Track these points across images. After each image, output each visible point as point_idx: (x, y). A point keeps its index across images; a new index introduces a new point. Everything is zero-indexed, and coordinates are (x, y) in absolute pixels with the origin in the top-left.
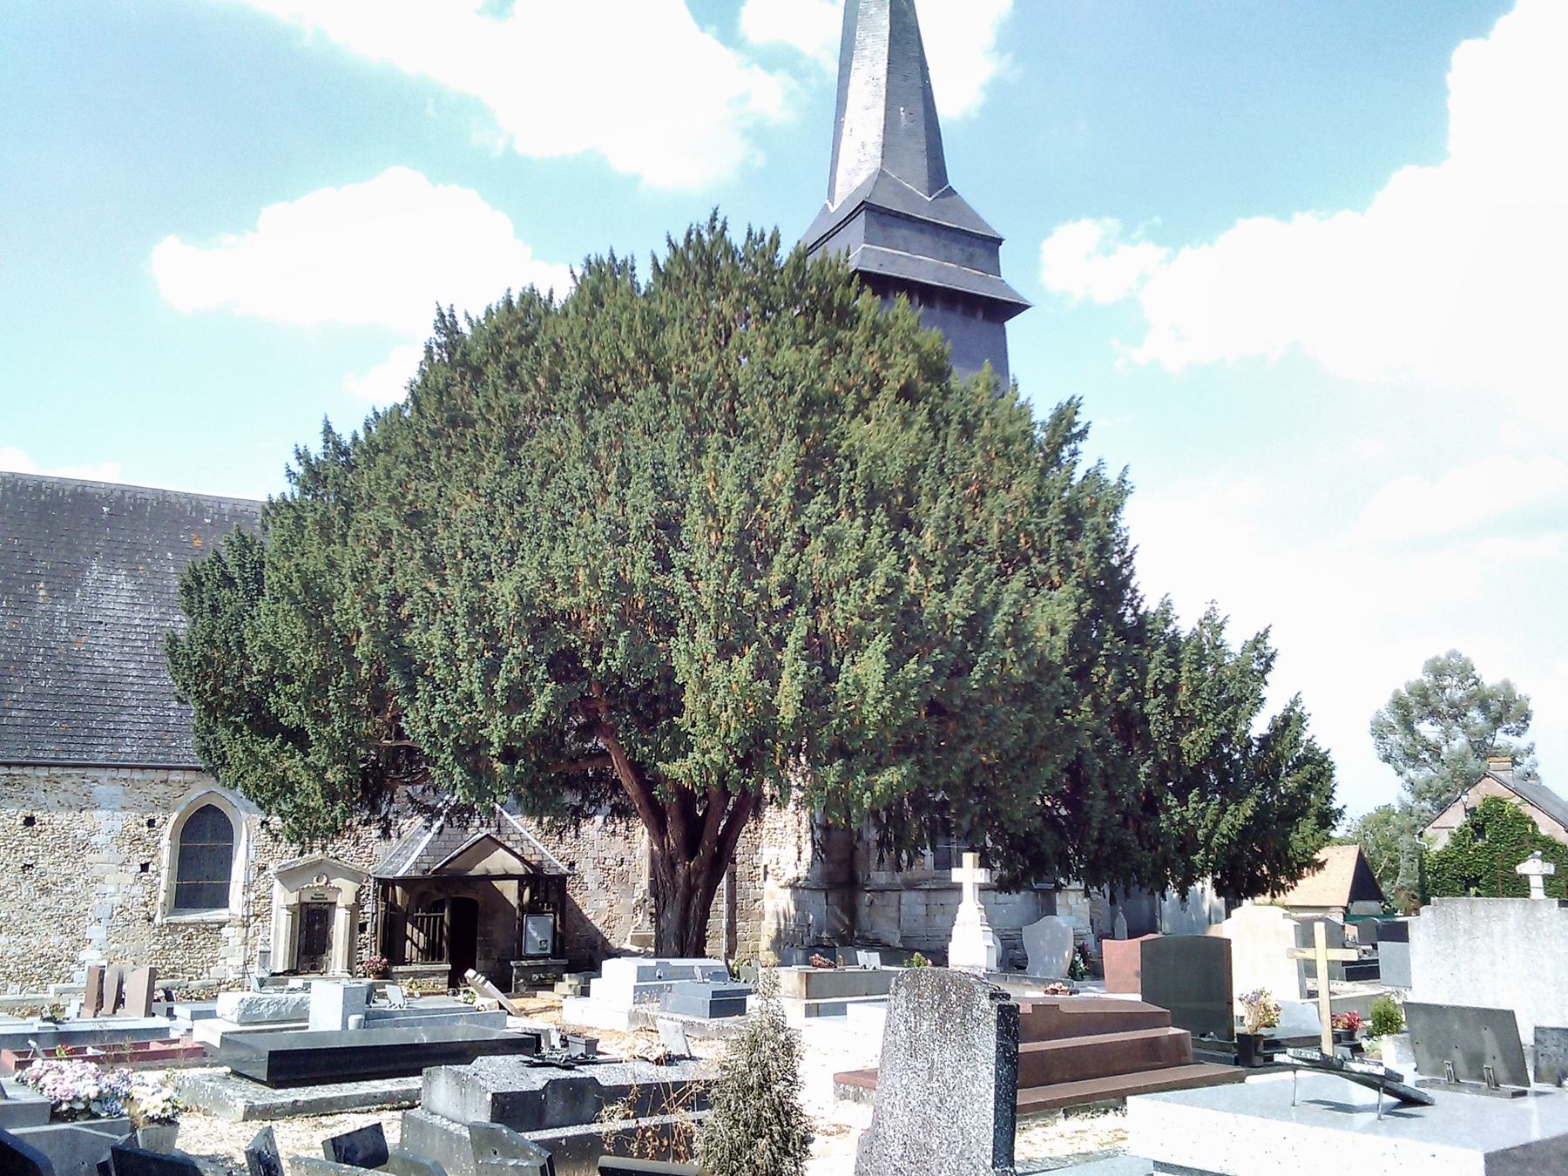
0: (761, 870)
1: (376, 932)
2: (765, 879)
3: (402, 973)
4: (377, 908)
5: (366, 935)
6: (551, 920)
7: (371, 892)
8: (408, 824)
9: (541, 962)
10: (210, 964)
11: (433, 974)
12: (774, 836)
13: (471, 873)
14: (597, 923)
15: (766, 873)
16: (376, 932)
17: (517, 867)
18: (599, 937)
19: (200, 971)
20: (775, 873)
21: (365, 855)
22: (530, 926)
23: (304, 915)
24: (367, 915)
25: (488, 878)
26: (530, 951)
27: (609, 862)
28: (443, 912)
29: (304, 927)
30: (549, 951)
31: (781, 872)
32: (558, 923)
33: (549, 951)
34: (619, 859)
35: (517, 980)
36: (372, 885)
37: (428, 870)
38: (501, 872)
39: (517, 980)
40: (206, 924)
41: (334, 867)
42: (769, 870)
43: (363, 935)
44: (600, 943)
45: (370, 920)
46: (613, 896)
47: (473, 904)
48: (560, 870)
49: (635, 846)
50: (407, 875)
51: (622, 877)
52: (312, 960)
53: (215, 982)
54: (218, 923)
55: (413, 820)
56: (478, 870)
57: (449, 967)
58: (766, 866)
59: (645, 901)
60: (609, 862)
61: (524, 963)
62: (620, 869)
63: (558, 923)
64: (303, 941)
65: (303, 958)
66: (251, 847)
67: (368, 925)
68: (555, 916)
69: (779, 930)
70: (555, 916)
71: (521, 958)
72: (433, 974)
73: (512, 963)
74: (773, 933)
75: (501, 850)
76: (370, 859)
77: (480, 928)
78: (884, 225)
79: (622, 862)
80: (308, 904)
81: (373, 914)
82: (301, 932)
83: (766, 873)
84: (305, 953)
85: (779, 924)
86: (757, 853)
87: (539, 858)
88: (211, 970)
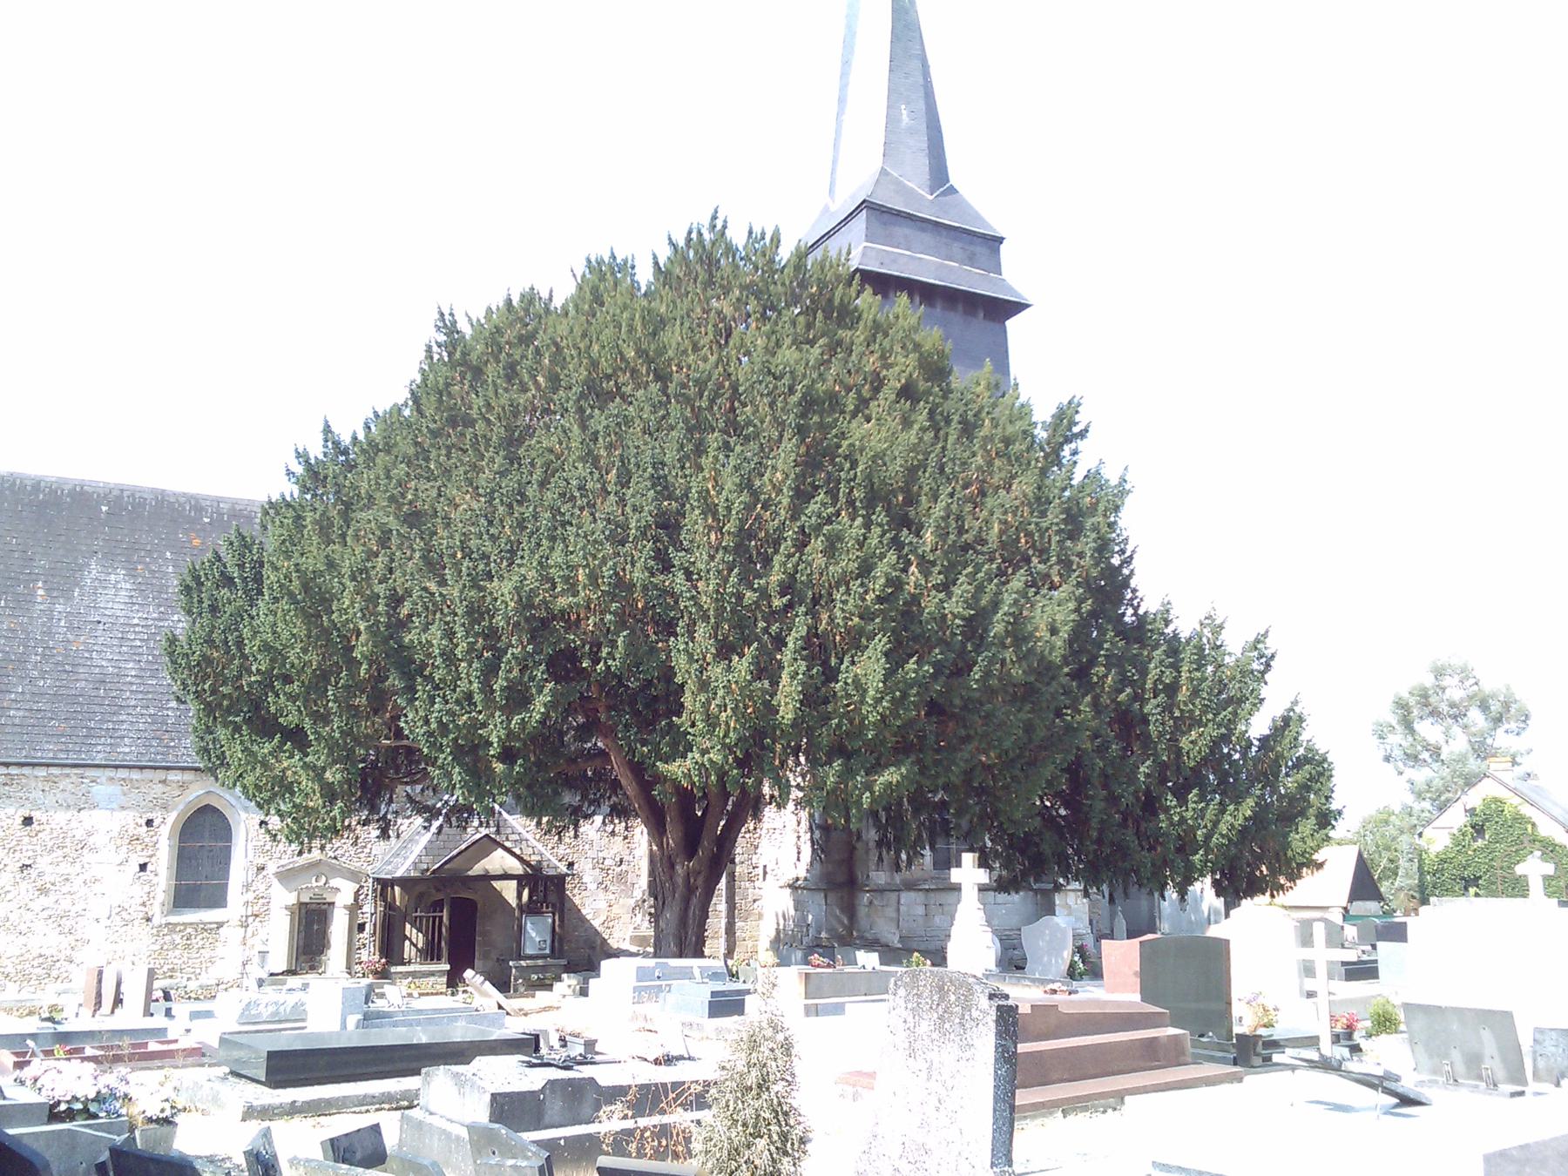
0: (760, 871)
2: (764, 879)
4: (376, 908)
7: (370, 892)
8: (407, 825)
9: (540, 962)
10: (209, 964)
11: (432, 974)
13: (470, 873)
14: (596, 923)
15: (765, 873)
16: (375, 933)
17: (516, 867)
19: (198, 971)
20: (774, 873)
21: (363, 855)
22: (529, 925)
25: (487, 878)
26: (529, 951)
28: (442, 911)
29: (302, 928)
32: (557, 923)
33: (547, 951)
34: (618, 859)
35: (516, 980)
36: (371, 885)
38: (500, 872)
39: (516, 980)
40: (205, 924)
42: (768, 870)
43: (361, 935)
44: (599, 942)
46: (612, 897)
47: (472, 905)
48: (559, 870)
49: (634, 846)
50: (406, 875)
51: (621, 877)
53: (214, 982)
54: (217, 923)
55: (411, 820)
56: (477, 870)
57: (448, 967)
58: (765, 866)
59: (644, 901)
61: (523, 963)
62: (619, 869)
63: (557, 923)
64: (301, 943)
65: (302, 958)
67: (367, 926)
69: (778, 931)
72: (432, 974)
73: (511, 963)
74: (773, 934)
75: (500, 851)
79: (621, 861)
80: (307, 904)
81: (372, 914)
83: (765, 873)
85: (778, 924)
87: (539, 858)
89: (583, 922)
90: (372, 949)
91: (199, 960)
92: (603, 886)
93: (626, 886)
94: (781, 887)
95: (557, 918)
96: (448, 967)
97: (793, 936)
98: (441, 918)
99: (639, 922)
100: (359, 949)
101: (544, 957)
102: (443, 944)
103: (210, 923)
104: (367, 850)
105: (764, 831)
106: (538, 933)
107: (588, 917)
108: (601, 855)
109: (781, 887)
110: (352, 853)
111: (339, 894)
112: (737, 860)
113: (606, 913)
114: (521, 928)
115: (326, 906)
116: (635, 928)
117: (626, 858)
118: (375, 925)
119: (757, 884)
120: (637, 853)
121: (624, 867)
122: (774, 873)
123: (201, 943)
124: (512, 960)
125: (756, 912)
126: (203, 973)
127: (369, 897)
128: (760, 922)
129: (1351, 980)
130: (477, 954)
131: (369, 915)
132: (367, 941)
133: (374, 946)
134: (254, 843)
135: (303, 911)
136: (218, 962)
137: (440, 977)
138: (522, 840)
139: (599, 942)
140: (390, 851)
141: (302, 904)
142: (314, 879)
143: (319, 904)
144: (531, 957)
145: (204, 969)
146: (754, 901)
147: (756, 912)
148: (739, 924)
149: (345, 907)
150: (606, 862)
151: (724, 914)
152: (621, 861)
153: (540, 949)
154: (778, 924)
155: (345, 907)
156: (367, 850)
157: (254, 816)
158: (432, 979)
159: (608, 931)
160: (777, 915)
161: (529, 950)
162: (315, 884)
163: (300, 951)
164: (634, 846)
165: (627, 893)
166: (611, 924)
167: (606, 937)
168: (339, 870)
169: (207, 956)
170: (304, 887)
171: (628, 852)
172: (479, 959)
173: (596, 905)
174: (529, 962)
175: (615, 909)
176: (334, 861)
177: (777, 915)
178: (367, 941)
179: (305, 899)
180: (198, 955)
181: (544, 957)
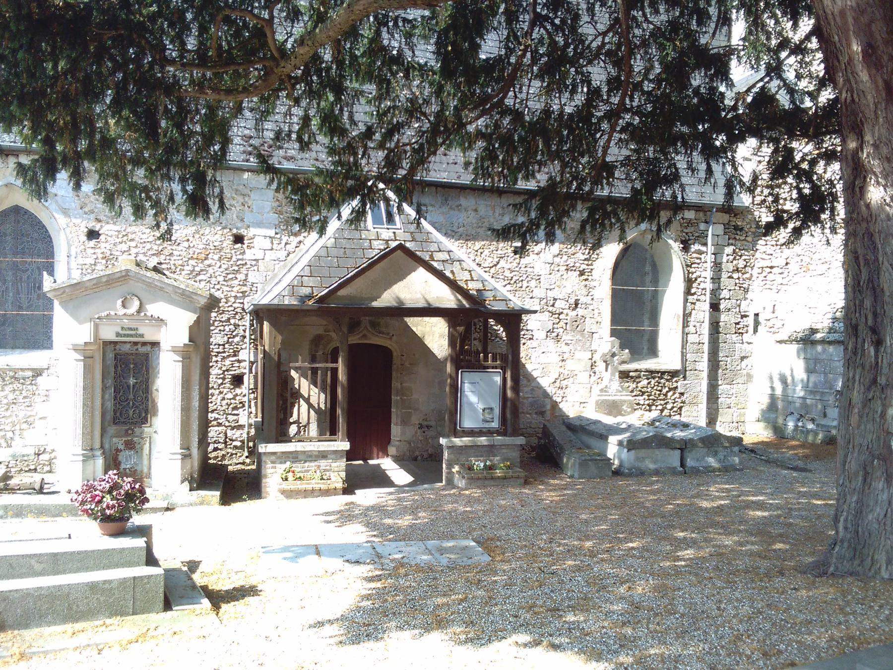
0: (750, 321)
1: (256, 388)
2: (755, 331)
3: (274, 454)
4: (256, 355)
5: (244, 389)
6: (498, 379)
7: (247, 334)
8: (294, 244)
9: (483, 440)
10: (25, 426)
11: (323, 455)
12: (770, 277)
13: (375, 304)
14: (545, 382)
15: (757, 324)
16: (256, 388)
17: (446, 298)
18: (547, 401)
19: (10, 434)
20: (770, 324)
21: (236, 282)
22: (467, 386)
23: (111, 361)
24: (242, 364)
25: (401, 312)
26: (468, 423)
27: (560, 304)
28: (337, 362)
29: (110, 382)
30: (495, 425)
31: (778, 324)
32: (509, 383)
33: (495, 425)
34: (572, 301)
35: (450, 466)
36: (248, 324)
37: (310, 297)
38: (421, 304)
39: (450, 466)
40: (15, 371)
41: (150, 285)
42: (761, 319)
43: (238, 391)
44: (548, 407)
45: (247, 371)
46: (566, 349)
47: (385, 354)
48: (511, 305)
49: (592, 284)
50: (276, 302)
51: (577, 324)
52: (126, 434)
53: (31, 451)
54: (32, 370)
55: (301, 238)
56: (386, 299)
57: (346, 446)
58: (757, 315)
59: (614, 355)
60: (560, 304)
61: (457, 441)
62: (574, 313)
63: (509, 383)
64: (110, 405)
65: (112, 430)
66: (73, 265)
67: (246, 378)
68: (504, 373)
69: (773, 397)
70: (504, 373)
71: (456, 434)
72: (323, 455)
73: (443, 441)
74: (765, 401)
75: (421, 272)
76: (244, 289)
77: (395, 384)
78: (466, 198)
79: (577, 304)
80: (115, 343)
81: (252, 363)
82: (104, 389)
83: (757, 324)
84: (115, 422)
85: (773, 388)
86: (746, 299)
87: (479, 286)
88: (25, 433)
89: (529, 380)
90: (253, 409)
91: (10, 420)
92: (555, 334)
93: (583, 335)
94: (780, 342)
95: (508, 375)
96: (346, 446)
97: (804, 405)
98: (335, 371)
99: (606, 382)
100: (235, 408)
101: (489, 432)
102: (339, 411)
103: (23, 370)
104: (241, 277)
105: (755, 272)
106: (480, 396)
107: (535, 374)
108: (551, 294)
109: (780, 342)
110: (221, 279)
111: (163, 329)
112: (722, 307)
113: (558, 370)
114: (455, 390)
115: (148, 348)
116: (602, 390)
117: (583, 300)
118: (256, 377)
119: (746, 337)
120: (597, 293)
121: (580, 311)
122: (770, 324)
123: (11, 396)
124: (444, 436)
125: (744, 372)
126: (17, 437)
127: (247, 340)
128: (749, 384)
129: (50, 338)
130: (394, 419)
131: (246, 364)
132: (246, 399)
133: (256, 403)
134: (80, 261)
135: (111, 356)
136: (38, 424)
137: (335, 460)
138: (453, 261)
139: (548, 407)
140: (273, 278)
141: (107, 343)
142: (119, 302)
143: (136, 343)
144: (471, 433)
145: (17, 433)
146: (743, 358)
147: (744, 372)
148: (723, 388)
149: (175, 350)
150: (558, 304)
151: (705, 375)
152: (577, 304)
153: (485, 421)
154: (773, 388)
155: (175, 350)
156: (241, 277)
157: (77, 221)
158: (323, 463)
159: (561, 392)
160: (771, 378)
161: (468, 423)
162: (122, 311)
163: (109, 416)
164: (592, 284)
165: (584, 343)
166: (564, 383)
167: (559, 400)
168: (161, 289)
169: (21, 415)
170: (103, 314)
171: (584, 292)
172: (396, 424)
173: (543, 359)
174: (466, 440)
175: (570, 365)
176: (157, 276)
177: (771, 378)
178: (246, 399)
179: (109, 333)
180: (8, 414)
181: (489, 432)
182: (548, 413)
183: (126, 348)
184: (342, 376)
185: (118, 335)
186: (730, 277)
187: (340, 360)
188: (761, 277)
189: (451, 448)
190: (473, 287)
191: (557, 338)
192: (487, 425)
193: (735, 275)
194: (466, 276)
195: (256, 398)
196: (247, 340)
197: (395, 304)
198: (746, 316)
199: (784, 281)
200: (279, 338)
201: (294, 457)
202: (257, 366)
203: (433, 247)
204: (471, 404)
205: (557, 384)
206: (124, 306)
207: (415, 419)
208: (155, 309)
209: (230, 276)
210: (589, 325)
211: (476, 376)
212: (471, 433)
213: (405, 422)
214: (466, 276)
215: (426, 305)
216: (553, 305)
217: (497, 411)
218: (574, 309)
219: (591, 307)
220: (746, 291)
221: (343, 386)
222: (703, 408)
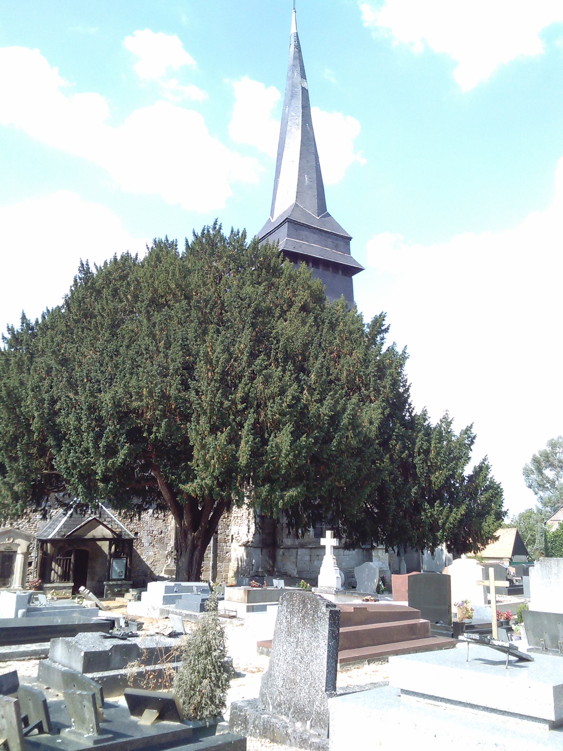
0: (230, 537)
2: (232, 542)
5: (32, 567)
7: (35, 546)
9: (119, 582)
11: (64, 588)
12: (237, 521)
13: (86, 537)
14: (148, 563)
15: (232, 539)
17: (109, 534)
20: (237, 539)
21: (33, 527)
22: (114, 564)
24: (32, 558)
25: (94, 540)
28: (71, 556)
31: (240, 539)
33: (123, 577)
34: (160, 531)
38: (101, 537)
39: (107, 591)
42: (234, 537)
43: (30, 568)
45: (34, 560)
46: (156, 550)
51: (161, 540)
55: (58, 510)
56: (90, 535)
58: (232, 535)
59: (172, 552)
61: (111, 583)
62: (160, 536)
67: (33, 563)
69: (238, 567)
72: (64, 588)
74: (235, 569)
76: (35, 529)
77: (89, 565)
81: (36, 557)
83: (232, 539)
90: (35, 575)
95: (128, 560)
96: (72, 584)
98: (71, 559)
105: (232, 518)
112: (219, 532)
116: (167, 566)
133: (36, 573)
139: (149, 573)
142: (7, 539)
143: (9, 552)
146: (227, 553)
148: (219, 564)
155: (22, 554)
161: (114, 576)
174: (114, 583)
178: (33, 571)
182: (149, 576)
183: (6, 553)
184: (72, 560)
185: (5, 549)
186: (222, 521)
187: (72, 556)
188: (234, 521)
189: (108, 585)
190: (118, 531)
191: (153, 546)
192: (120, 577)
193: (224, 520)
194: (116, 526)
195: (36, 571)
196: (35, 549)
197: (92, 537)
198: (228, 536)
199: (242, 523)
200: (54, 549)
201: (56, 588)
202: (38, 559)
203: (106, 516)
204: (115, 570)
205: (153, 564)
206: (8, 540)
207: (96, 578)
208: (17, 541)
209: (31, 525)
210: (166, 540)
211: (118, 560)
212: (114, 580)
213: (92, 579)
214: (116, 526)
215: (103, 537)
216: (152, 533)
217: (124, 572)
218: (160, 534)
219: (167, 534)
220: (228, 526)
221: (73, 564)
222: (210, 572)
